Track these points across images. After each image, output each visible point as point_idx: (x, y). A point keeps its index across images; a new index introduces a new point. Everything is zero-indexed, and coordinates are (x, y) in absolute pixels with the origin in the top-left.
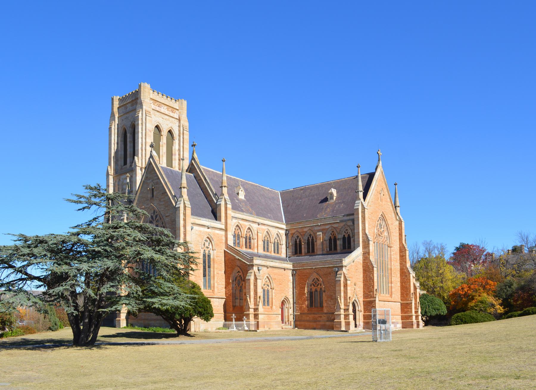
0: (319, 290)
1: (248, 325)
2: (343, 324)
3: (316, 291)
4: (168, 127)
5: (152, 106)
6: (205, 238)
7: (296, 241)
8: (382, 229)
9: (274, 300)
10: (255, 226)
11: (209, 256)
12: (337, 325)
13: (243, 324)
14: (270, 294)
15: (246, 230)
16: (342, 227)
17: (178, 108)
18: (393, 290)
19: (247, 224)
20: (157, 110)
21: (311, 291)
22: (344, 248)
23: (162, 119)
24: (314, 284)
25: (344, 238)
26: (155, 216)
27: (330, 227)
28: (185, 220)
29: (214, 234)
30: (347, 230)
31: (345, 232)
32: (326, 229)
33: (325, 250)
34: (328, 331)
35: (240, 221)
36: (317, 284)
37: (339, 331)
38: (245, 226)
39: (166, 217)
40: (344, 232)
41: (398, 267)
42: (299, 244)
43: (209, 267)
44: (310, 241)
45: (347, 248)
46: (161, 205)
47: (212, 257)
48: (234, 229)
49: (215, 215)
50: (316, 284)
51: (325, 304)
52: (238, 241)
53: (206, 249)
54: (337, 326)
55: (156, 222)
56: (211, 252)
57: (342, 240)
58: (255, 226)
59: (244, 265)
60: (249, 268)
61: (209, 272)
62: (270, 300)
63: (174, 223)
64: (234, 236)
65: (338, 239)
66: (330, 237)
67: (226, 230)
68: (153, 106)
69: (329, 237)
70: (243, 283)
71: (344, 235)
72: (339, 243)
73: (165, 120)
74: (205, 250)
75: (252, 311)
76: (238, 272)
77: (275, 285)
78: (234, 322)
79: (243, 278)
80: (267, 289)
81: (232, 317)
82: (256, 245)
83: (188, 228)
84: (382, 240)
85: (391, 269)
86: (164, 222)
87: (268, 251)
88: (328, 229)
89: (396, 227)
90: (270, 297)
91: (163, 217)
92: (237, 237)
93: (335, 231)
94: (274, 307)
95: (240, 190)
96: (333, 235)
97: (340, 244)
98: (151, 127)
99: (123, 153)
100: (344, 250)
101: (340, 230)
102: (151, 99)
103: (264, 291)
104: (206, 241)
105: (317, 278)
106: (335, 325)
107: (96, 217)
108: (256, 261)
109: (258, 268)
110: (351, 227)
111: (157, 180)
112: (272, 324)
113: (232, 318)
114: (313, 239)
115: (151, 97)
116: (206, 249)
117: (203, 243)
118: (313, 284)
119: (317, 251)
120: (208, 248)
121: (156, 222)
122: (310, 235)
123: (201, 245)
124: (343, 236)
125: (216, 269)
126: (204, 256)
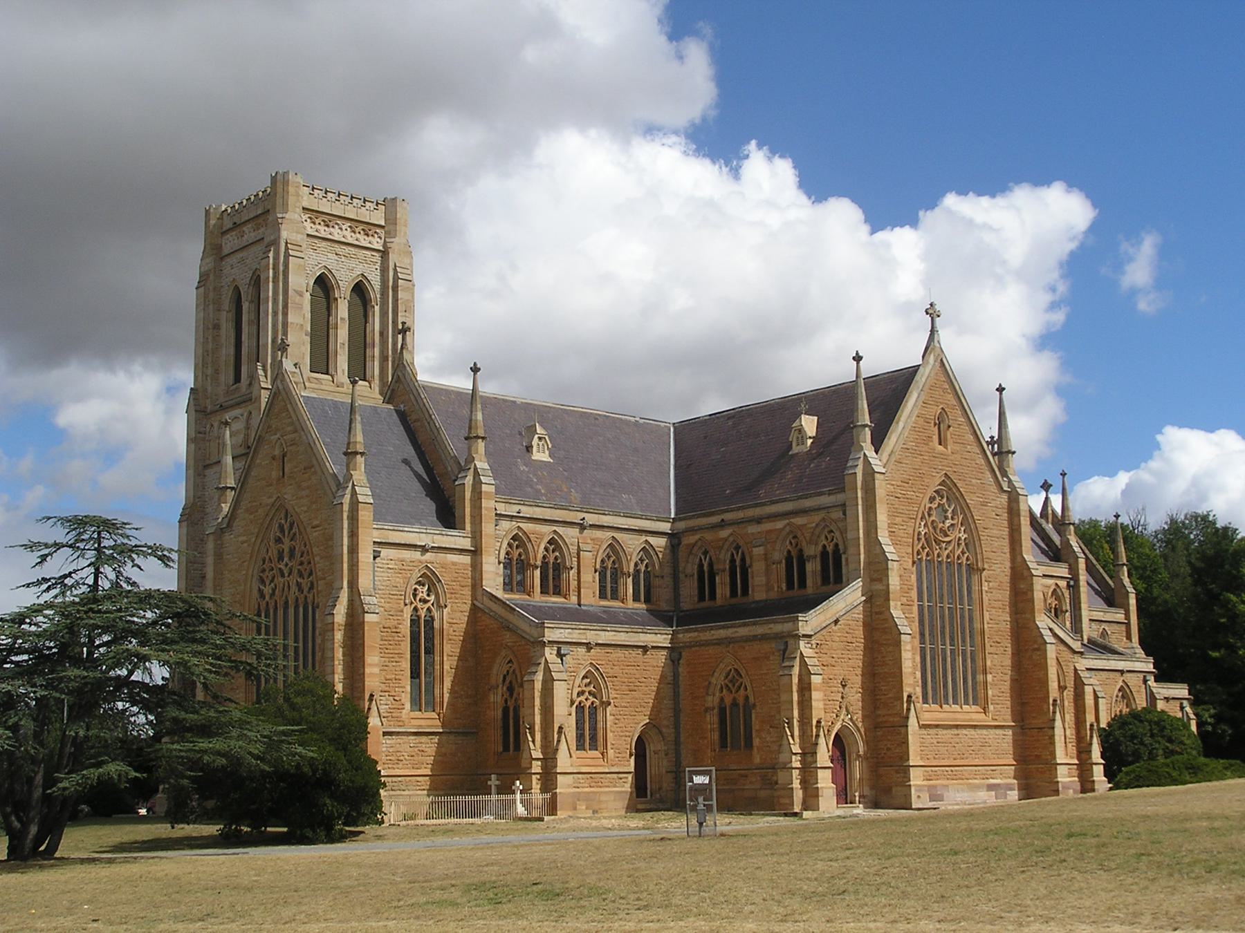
0: (741, 701)
1: (527, 804)
2: (798, 795)
3: (735, 704)
4: (354, 276)
5: (309, 228)
6: (416, 575)
7: (701, 565)
8: (948, 522)
9: (610, 735)
10: (570, 534)
11: (430, 622)
12: (783, 797)
13: (514, 801)
14: (600, 717)
15: (542, 546)
16: (817, 525)
17: (383, 224)
18: (990, 692)
19: (547, 529)
20: (323, 234)
21: (723, 706)
22: (825, 580)
23: (336, 257)
24: (730, 685)
25: (824, 554)
26: (288, 524)
27: (785, 526)
28: (353, 534)
29: (443, 566)
30: (832, 531)
31: (826, 537)
32: (776, 530)
33: (776, 589)
34: (751, 814)
35: (521, 525)
36: (737, 684)
37: (786, 815)
38: (542, 536)
39: (313, 528)
40: (823, 537)
41: (1006, 626)
42: (709, 572)
43: (430, 651)
44: (738, 563)
45: (831, 580)
46: (302, 497)
47: (436, 625)
48: (505, 545)
49: (448, 517)
50: (734, 686)
51: (756, 742)
52: (519, 578)
53: (420, 605)
54: (783, 801)
55: (292, 540)
56: (436, 614)
57: (818, 559)
58: (570, 534)
59: (523, 643)
60: (533, 650)
61: (431, 664)
62: (600, 733)
63: (330, 543)
64: (508, 564)
65: (810, 557)
66: (789, 552)
67: (476, 552)
68: (310, 228)
69: (785, 553)
70: (521, 690)
71: (824, 546)
72: (812, 567)
73: (343, 259)
74: (416, 609)
75: (536, 767)
76: (509, 662)
77: (613, 694)
78: (518, 796)
79: (519, 677)
80: (588, 704)
81: (489, 783)
82: (574, 584)
83: (365, 555)
84: (947, 552)
85: (983, 632)
86: (307, 543)
87: (615, 596)
88: (782, 529)
89: (999, 511)
90: (600, 725)
91: (305, 529)
92: (516, 568)
93: (799, 535)
94: (611, 752)
95: (536, 436)
96: (797, 545)
97: (814, 572)
98: (300, 281)
99: (232, 351)
100: (824, 587)
101: (813, 534)
102: (304, 208)
103: (580, 708)
104: (419, 583)
105: (736, 670)
106: (779, 797)
107: (72, 570)
108: (554, 633)
109: (559, 650)
110: (840, 525)
111: (293, 436)
112: (603, 798)
113: (491, 786)
114: (743, 560)
115: (306, 204)
116: (420, 605)
117: (410, 592)
118: (727, 686)
119: (753, 590)
120: (425, 601)
121: (292, 540)
122: (738, 548)
123: (403, 597)
124: (820, 548)
125: (448, 655)
126: (415, 622)
